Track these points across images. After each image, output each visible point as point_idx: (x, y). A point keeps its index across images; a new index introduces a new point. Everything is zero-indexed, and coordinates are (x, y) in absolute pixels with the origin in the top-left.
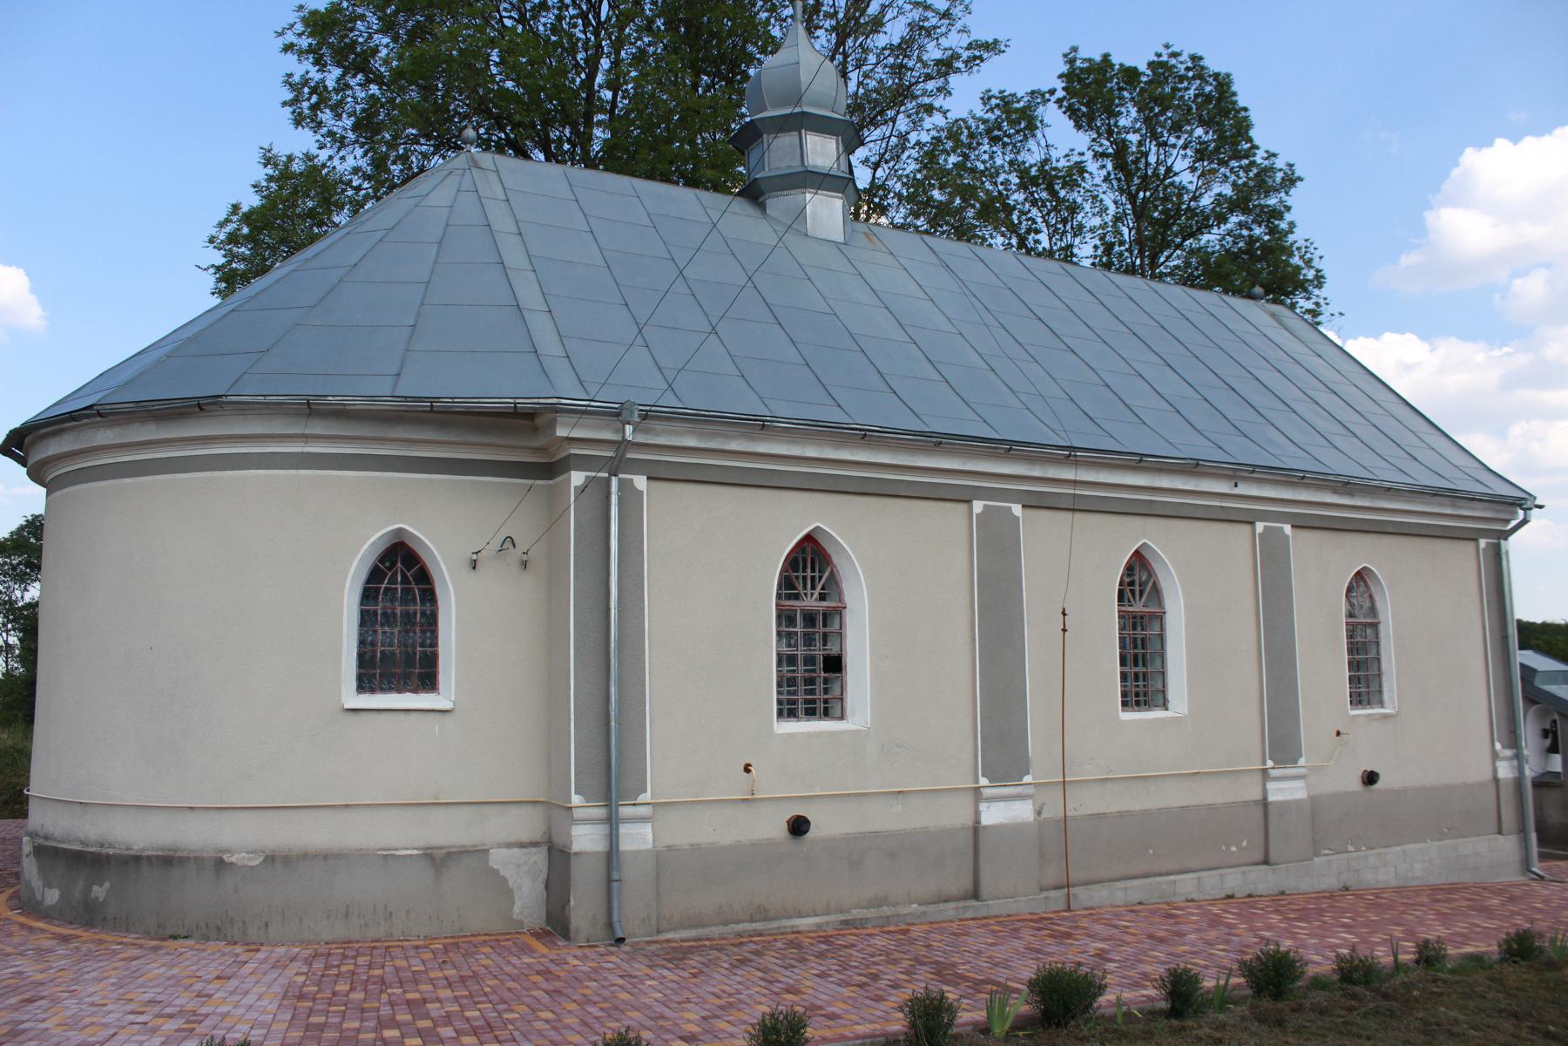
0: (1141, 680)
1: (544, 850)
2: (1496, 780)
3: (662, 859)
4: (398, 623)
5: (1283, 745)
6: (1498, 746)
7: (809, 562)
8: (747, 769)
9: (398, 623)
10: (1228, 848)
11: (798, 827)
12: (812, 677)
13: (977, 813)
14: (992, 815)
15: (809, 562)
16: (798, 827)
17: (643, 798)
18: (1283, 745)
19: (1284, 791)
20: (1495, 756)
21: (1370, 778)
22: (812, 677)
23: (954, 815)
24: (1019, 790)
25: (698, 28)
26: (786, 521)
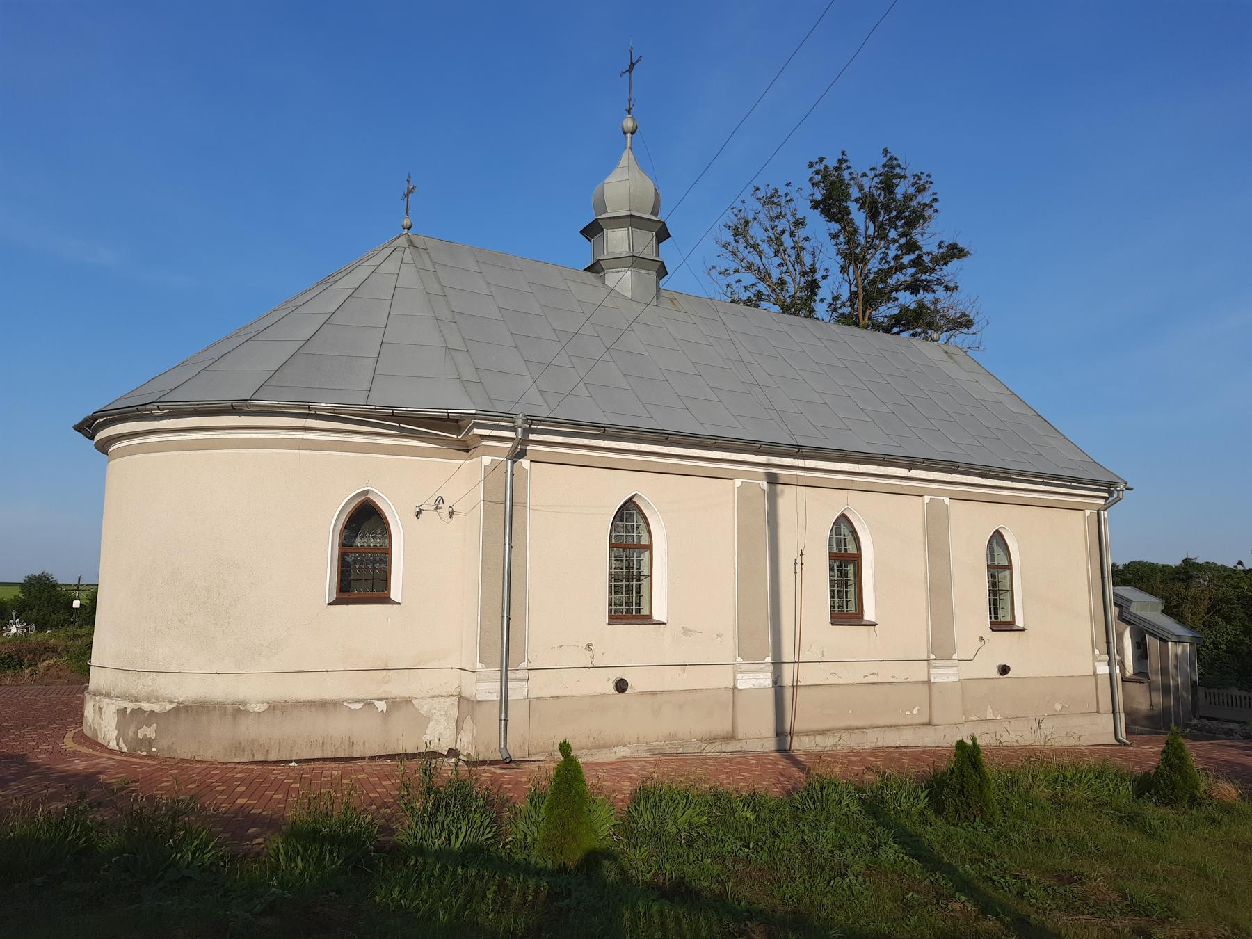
0: (846, 610)
1: (455, 700)
2: (1095, 675)
3: (534, 702)
4: (362, 564)
5: (942, 647)
6: (1097, 652)
7: (628, 514)
8: (589, 647)
9: (362, 564)
10: (904, 712)
11: (621, 686)
12: (627, 598)
13: (735, 680)
14: (744, 682)
15: (628, 514)
16: (621, 686)
17: (522, 665)
18: (942, 647)
19: (944, 675)
20: (1094, 658)
21: (1004, 670)
22: (627, 598)
23: (719, 679)
24: (762, 666)
25: (1235, 643)
26: (613, 489)
